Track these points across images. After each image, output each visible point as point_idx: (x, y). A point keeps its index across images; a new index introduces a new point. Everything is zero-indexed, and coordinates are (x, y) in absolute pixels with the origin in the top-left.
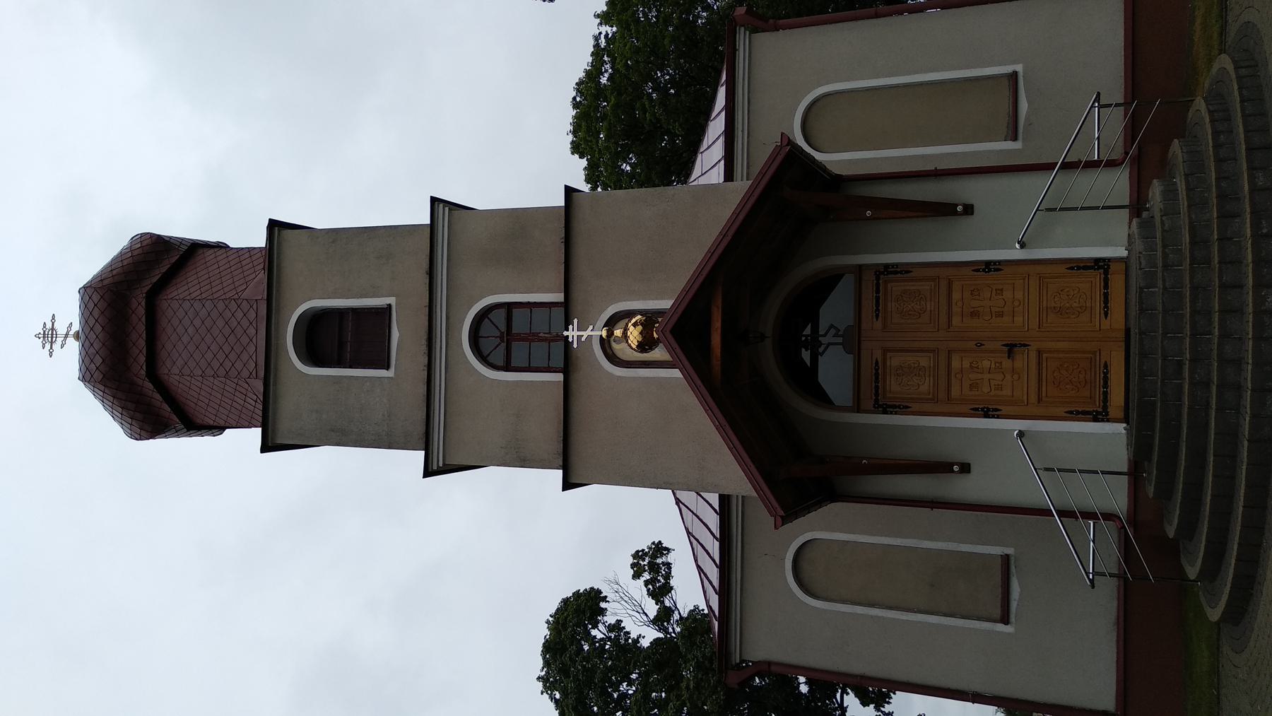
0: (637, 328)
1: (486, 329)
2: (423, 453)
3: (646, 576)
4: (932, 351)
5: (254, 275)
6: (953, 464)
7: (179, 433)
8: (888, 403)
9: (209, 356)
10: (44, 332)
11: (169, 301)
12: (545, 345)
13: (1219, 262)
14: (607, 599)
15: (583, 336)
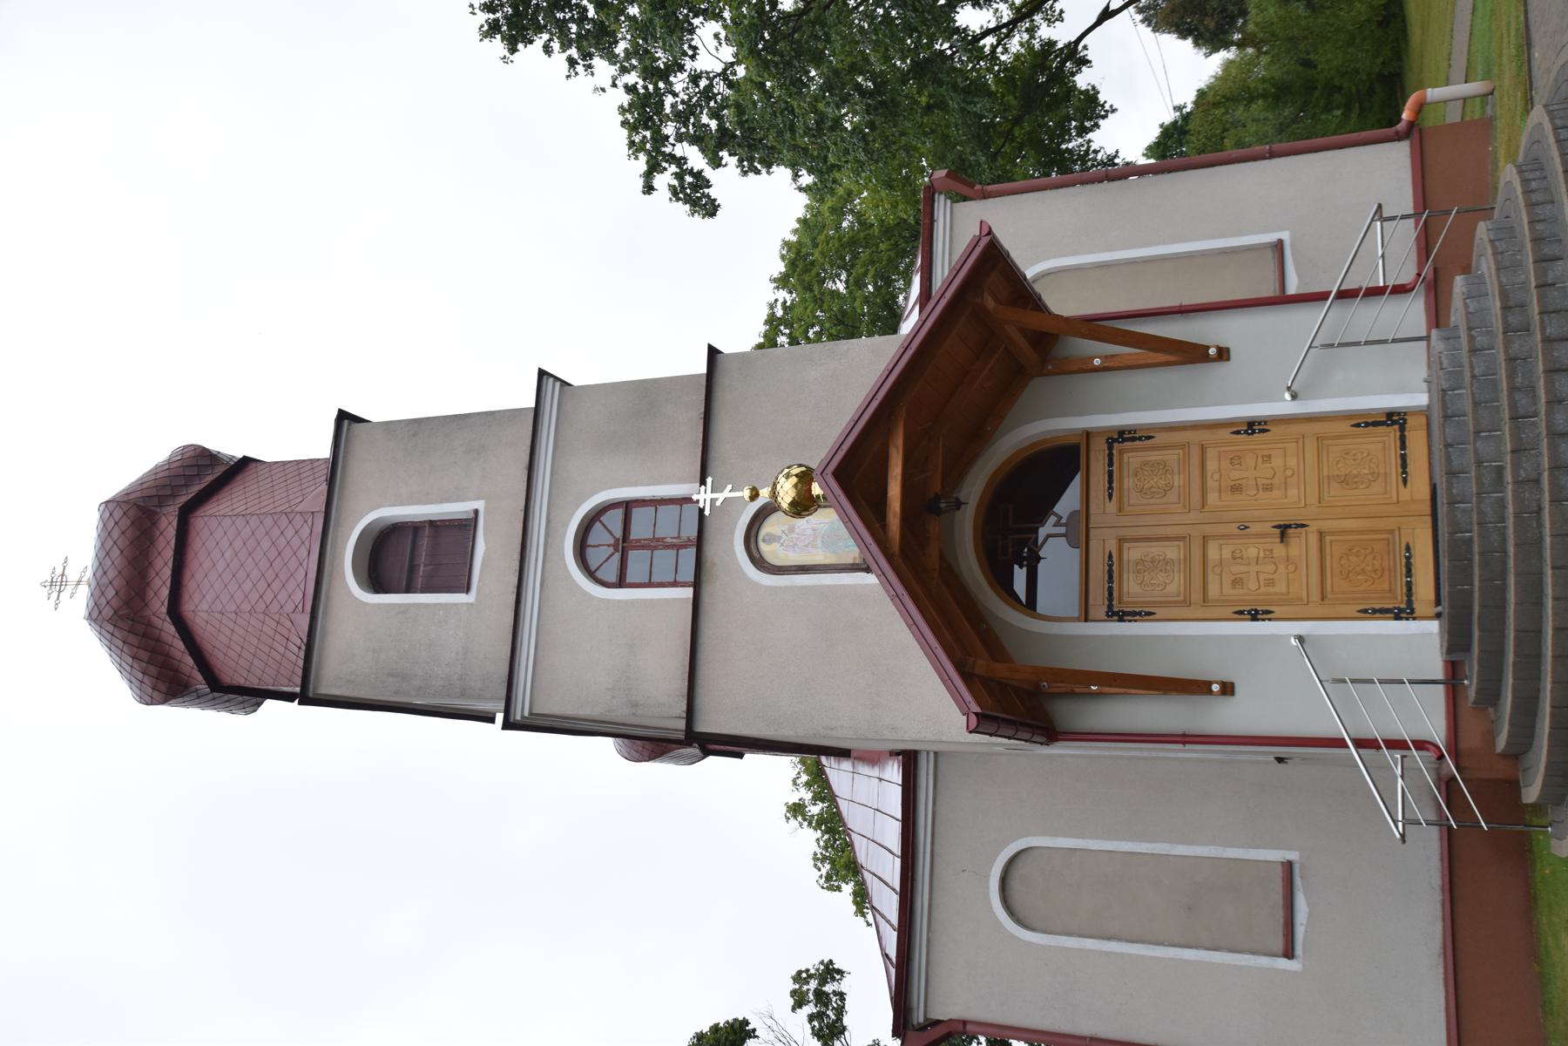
0: (790, 479)
1: (598, 535)
3: (810, 1009)
4: (1182, 538)
5: (313, 488)
6: (1210, 683)
7: (201, 700)
8: (1126, 610)
9: (248, 586)
11: (206, 519)
13: (1541, 313)
15: (717, 499)
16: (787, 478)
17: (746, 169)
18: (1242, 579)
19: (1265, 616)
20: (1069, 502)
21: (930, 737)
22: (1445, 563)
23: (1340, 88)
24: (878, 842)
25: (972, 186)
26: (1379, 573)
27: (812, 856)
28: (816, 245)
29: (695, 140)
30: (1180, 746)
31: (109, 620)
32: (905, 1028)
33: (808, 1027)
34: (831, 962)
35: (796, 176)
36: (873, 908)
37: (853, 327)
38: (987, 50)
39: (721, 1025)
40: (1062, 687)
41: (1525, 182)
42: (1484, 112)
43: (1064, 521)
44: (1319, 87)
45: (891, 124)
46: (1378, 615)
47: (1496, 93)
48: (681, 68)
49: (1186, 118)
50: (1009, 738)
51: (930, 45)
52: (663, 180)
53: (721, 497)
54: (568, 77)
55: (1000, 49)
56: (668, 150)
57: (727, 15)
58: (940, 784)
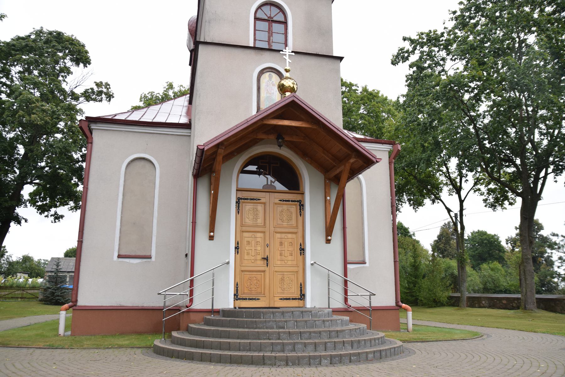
1: (275, 10)
3: (96, 89)
6: (213, 232)
8: (240, 204)
12: (267, 39)
13: (335, 342)
16: (293, 83)
17: (408, 77)
18: (250, 244)
19: (236, 251)
20: (279, 186)
21: (196, 133)
22: (253, 310)
23: (415, 286)
24: (158, 114)
25: (394, 158)
26: (250, 290)
27: (153, 91)
28: (377, 103)
29: (421, 58)
30: (191, 221)
32: (89, 121)
33: (89, 88)
34: (113, 97)
35: (403, 96)
36: (133, 111)
37: (347, 114)
38: (441, 168)
39: (88, 54)
40: (213, 179)
41: (378, 339)
42: (402, 329)
43: (273, 184)
44: (416, 280)
45: (419, 132)
46: (236, 289)
47: (408, 332)
48: (448, 55)
49: (410, 236)
50: (195, 161)
51: (446, 149)
52: (407, 46)
53: (287, 57)
55: (441, 173)
56: (418, 47)
57: (465, 73)
58: (179, 137)
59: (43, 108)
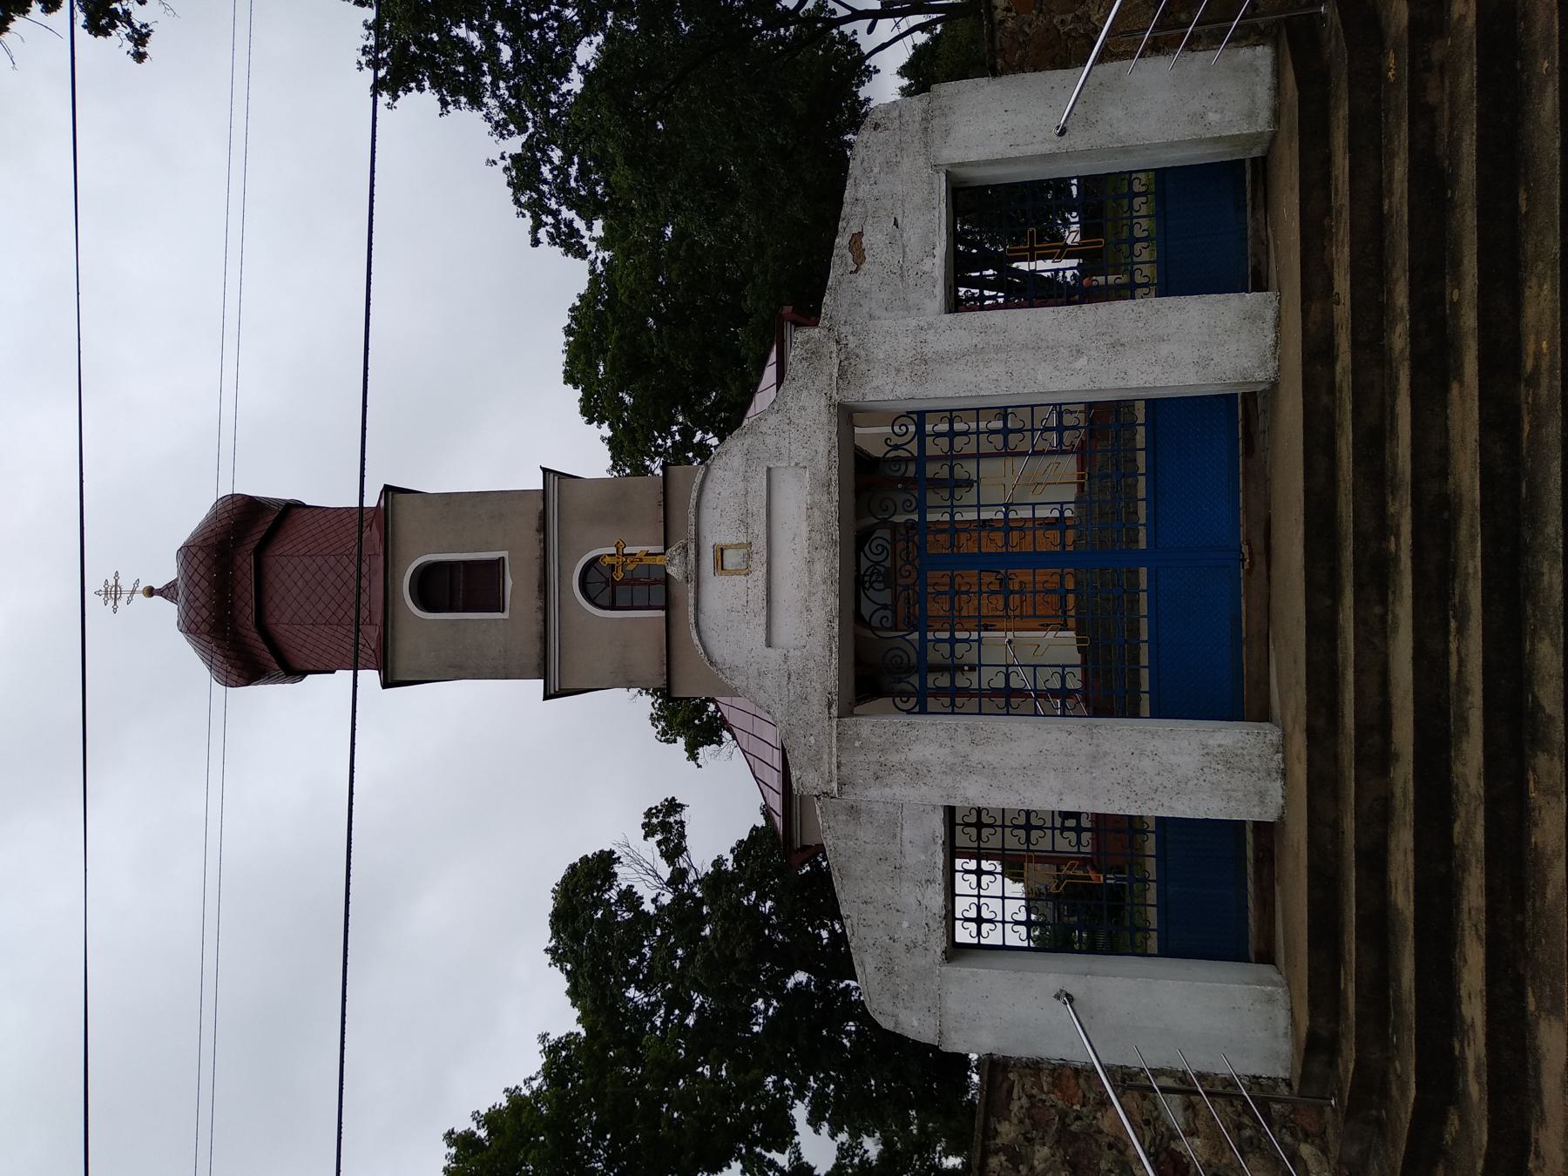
2: (541, 682)
3: (659, 837)
9: (321, 606)
10: (106, 589)
11: (277, 558)
14: (621, 860)
31: (208, 634)
54: (440, 115)
59: (719, 936)
